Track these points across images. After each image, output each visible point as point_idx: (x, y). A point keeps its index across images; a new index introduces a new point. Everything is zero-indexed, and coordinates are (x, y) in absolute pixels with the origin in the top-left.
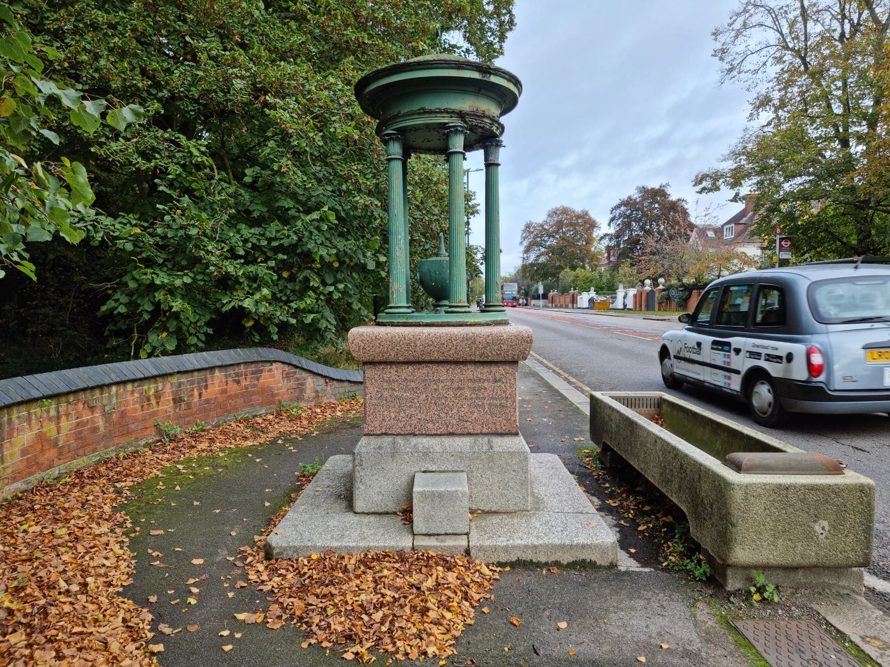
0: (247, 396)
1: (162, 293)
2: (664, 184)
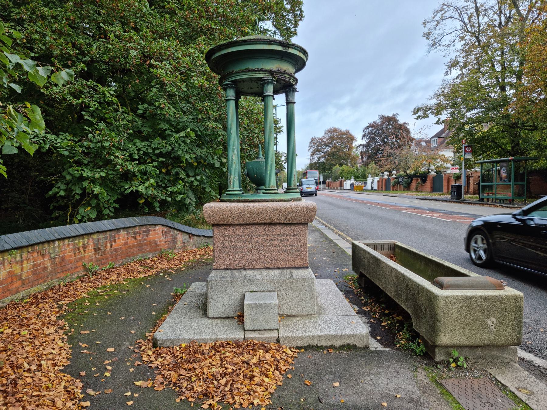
0: (140, 246)
2: (395, 113)
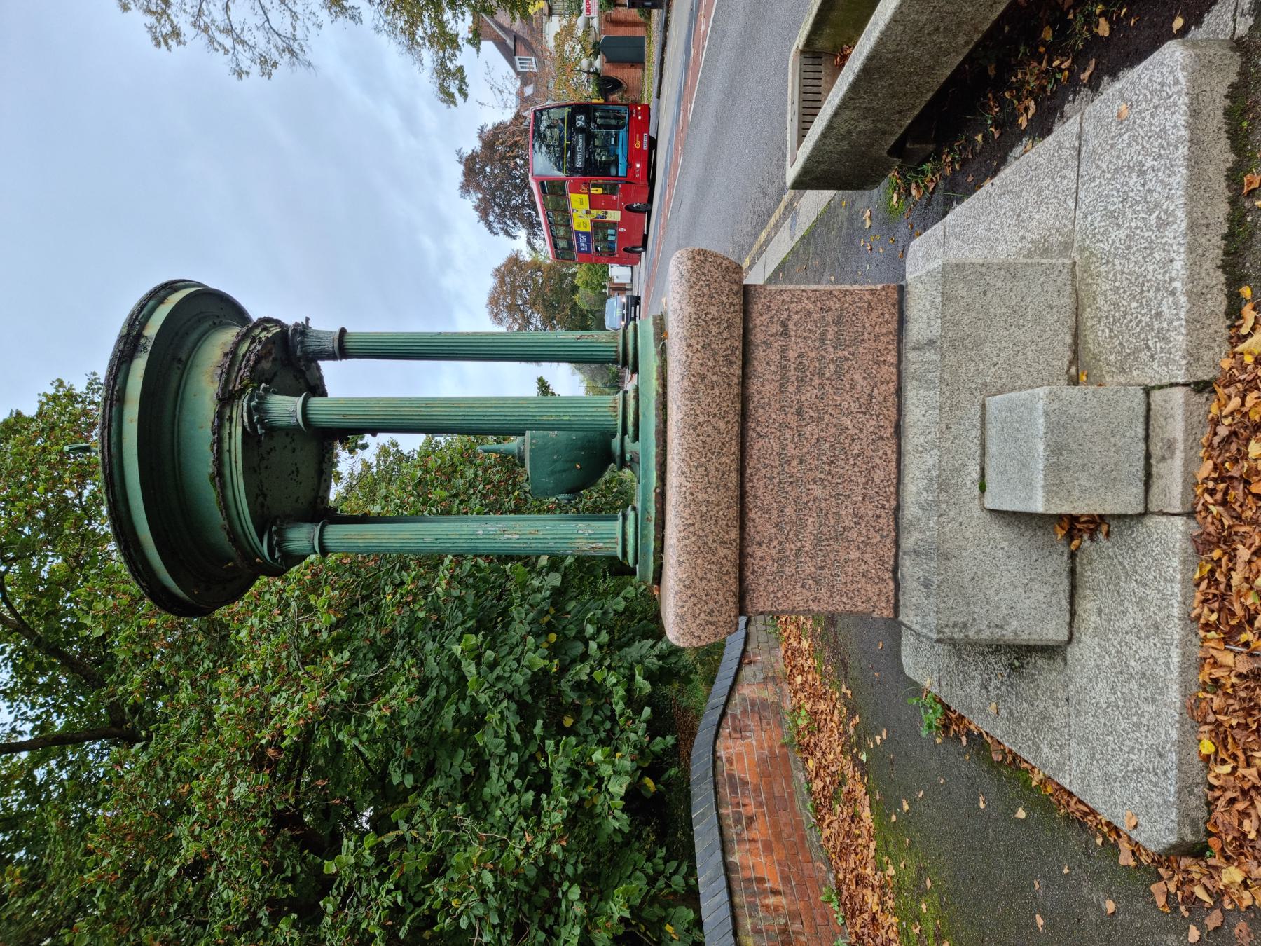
0: (775, 805)
1: (598, 936)
2: (457, 158)
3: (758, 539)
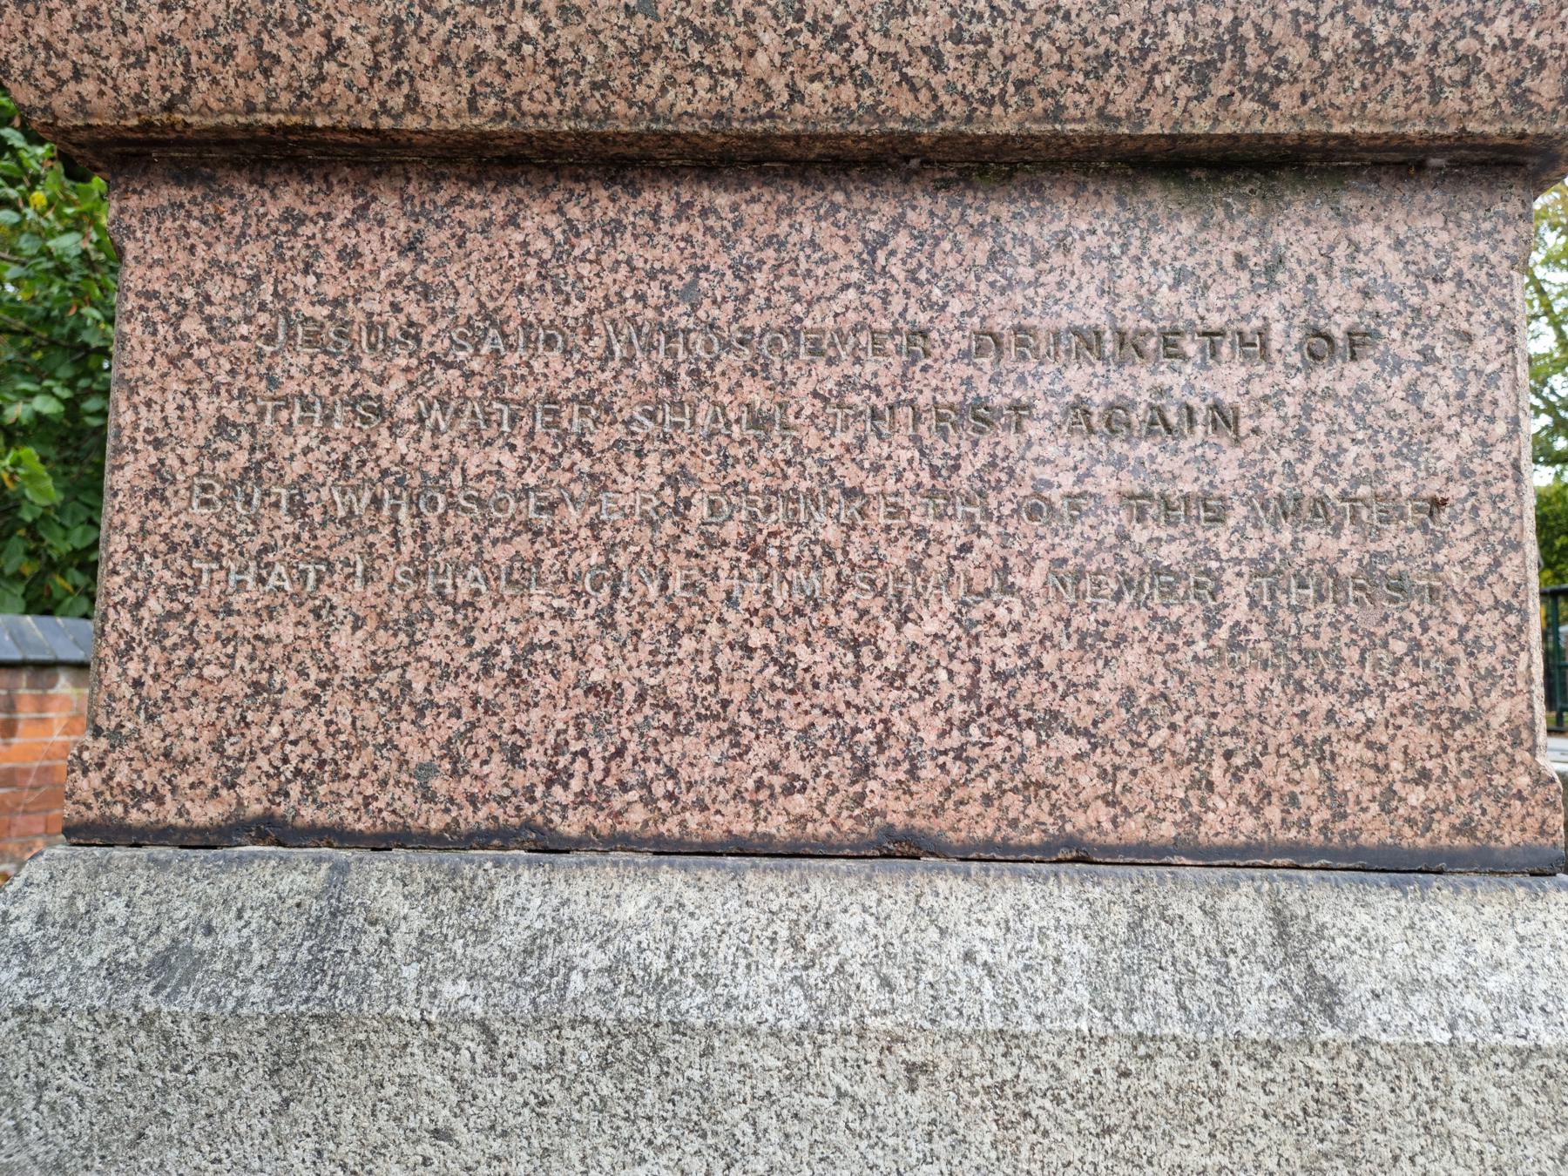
3: (434, 238)
